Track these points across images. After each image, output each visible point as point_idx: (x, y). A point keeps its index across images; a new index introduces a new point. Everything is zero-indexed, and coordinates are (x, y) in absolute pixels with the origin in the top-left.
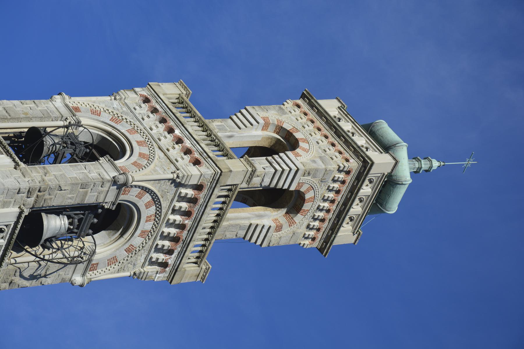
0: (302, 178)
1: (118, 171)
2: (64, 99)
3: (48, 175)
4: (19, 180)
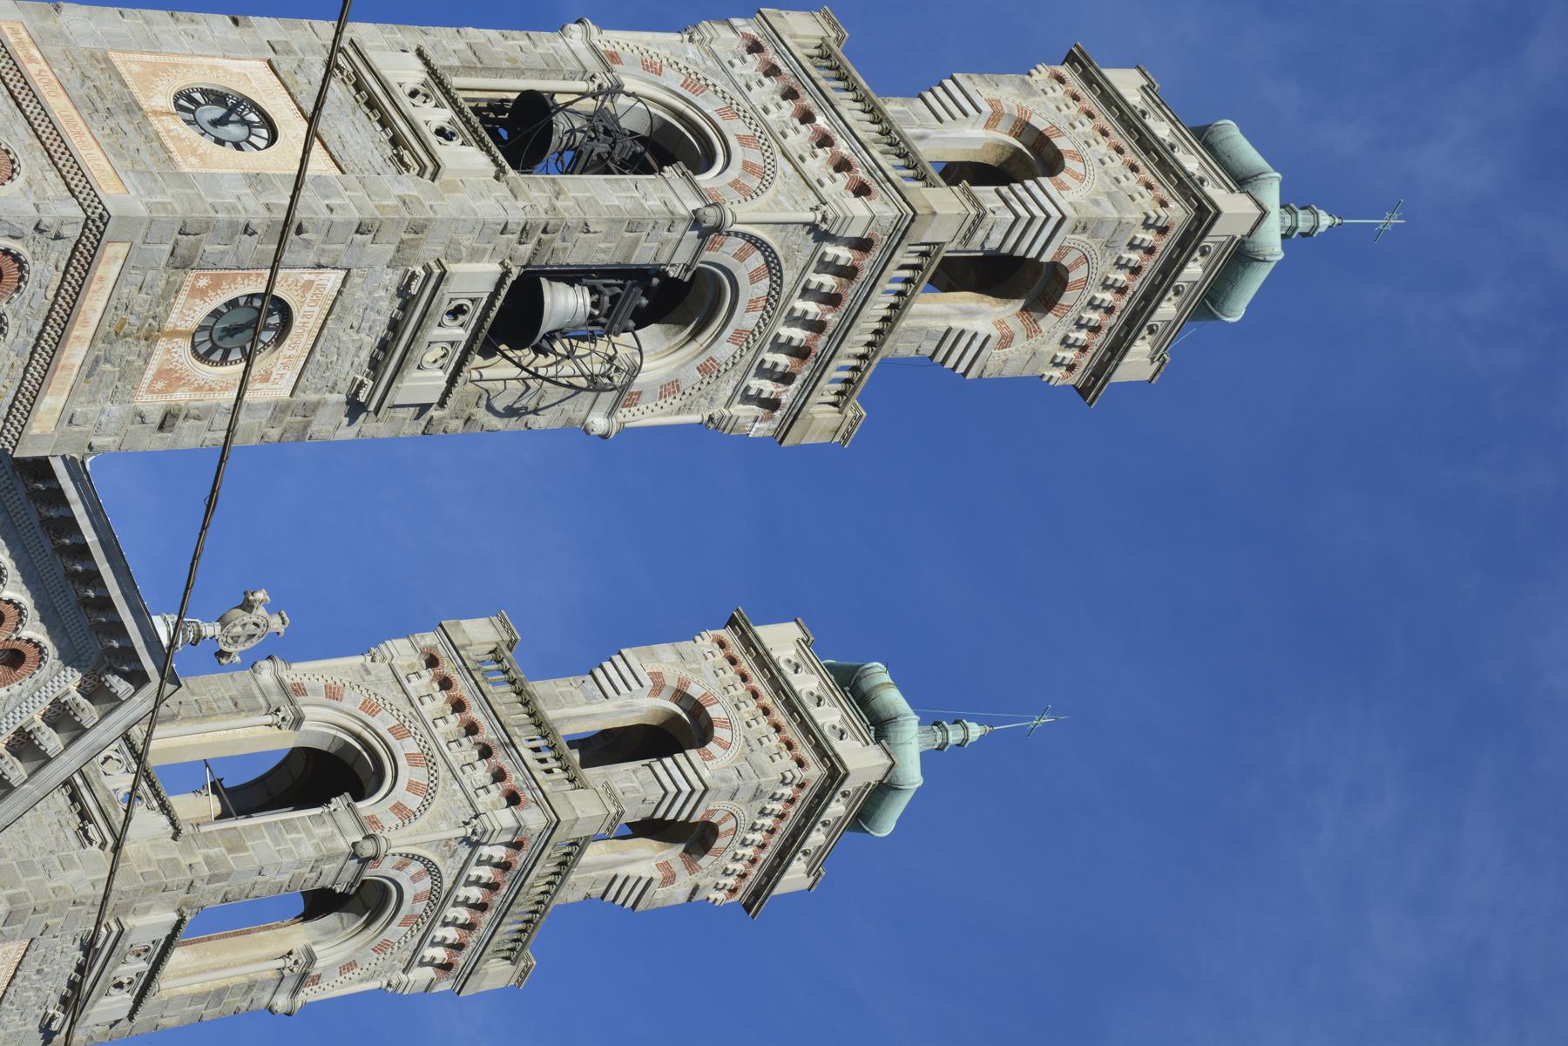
0: (1068, 236)
1: (703, 198)
2: (588, 33)
3: (562, 197)
4: (506, 204)
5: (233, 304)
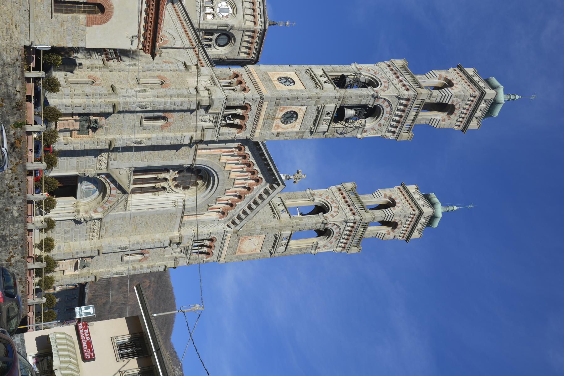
1: (375, 92)
2: (355, 65)
5: (287, 113)
